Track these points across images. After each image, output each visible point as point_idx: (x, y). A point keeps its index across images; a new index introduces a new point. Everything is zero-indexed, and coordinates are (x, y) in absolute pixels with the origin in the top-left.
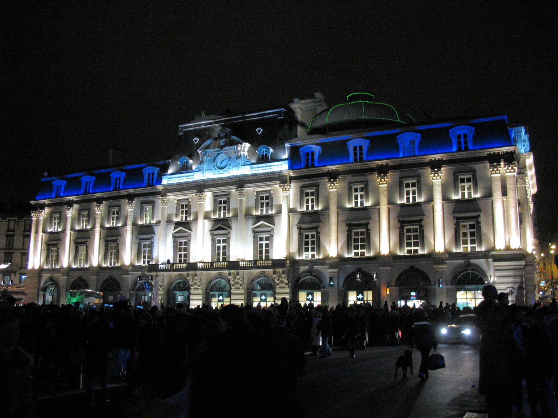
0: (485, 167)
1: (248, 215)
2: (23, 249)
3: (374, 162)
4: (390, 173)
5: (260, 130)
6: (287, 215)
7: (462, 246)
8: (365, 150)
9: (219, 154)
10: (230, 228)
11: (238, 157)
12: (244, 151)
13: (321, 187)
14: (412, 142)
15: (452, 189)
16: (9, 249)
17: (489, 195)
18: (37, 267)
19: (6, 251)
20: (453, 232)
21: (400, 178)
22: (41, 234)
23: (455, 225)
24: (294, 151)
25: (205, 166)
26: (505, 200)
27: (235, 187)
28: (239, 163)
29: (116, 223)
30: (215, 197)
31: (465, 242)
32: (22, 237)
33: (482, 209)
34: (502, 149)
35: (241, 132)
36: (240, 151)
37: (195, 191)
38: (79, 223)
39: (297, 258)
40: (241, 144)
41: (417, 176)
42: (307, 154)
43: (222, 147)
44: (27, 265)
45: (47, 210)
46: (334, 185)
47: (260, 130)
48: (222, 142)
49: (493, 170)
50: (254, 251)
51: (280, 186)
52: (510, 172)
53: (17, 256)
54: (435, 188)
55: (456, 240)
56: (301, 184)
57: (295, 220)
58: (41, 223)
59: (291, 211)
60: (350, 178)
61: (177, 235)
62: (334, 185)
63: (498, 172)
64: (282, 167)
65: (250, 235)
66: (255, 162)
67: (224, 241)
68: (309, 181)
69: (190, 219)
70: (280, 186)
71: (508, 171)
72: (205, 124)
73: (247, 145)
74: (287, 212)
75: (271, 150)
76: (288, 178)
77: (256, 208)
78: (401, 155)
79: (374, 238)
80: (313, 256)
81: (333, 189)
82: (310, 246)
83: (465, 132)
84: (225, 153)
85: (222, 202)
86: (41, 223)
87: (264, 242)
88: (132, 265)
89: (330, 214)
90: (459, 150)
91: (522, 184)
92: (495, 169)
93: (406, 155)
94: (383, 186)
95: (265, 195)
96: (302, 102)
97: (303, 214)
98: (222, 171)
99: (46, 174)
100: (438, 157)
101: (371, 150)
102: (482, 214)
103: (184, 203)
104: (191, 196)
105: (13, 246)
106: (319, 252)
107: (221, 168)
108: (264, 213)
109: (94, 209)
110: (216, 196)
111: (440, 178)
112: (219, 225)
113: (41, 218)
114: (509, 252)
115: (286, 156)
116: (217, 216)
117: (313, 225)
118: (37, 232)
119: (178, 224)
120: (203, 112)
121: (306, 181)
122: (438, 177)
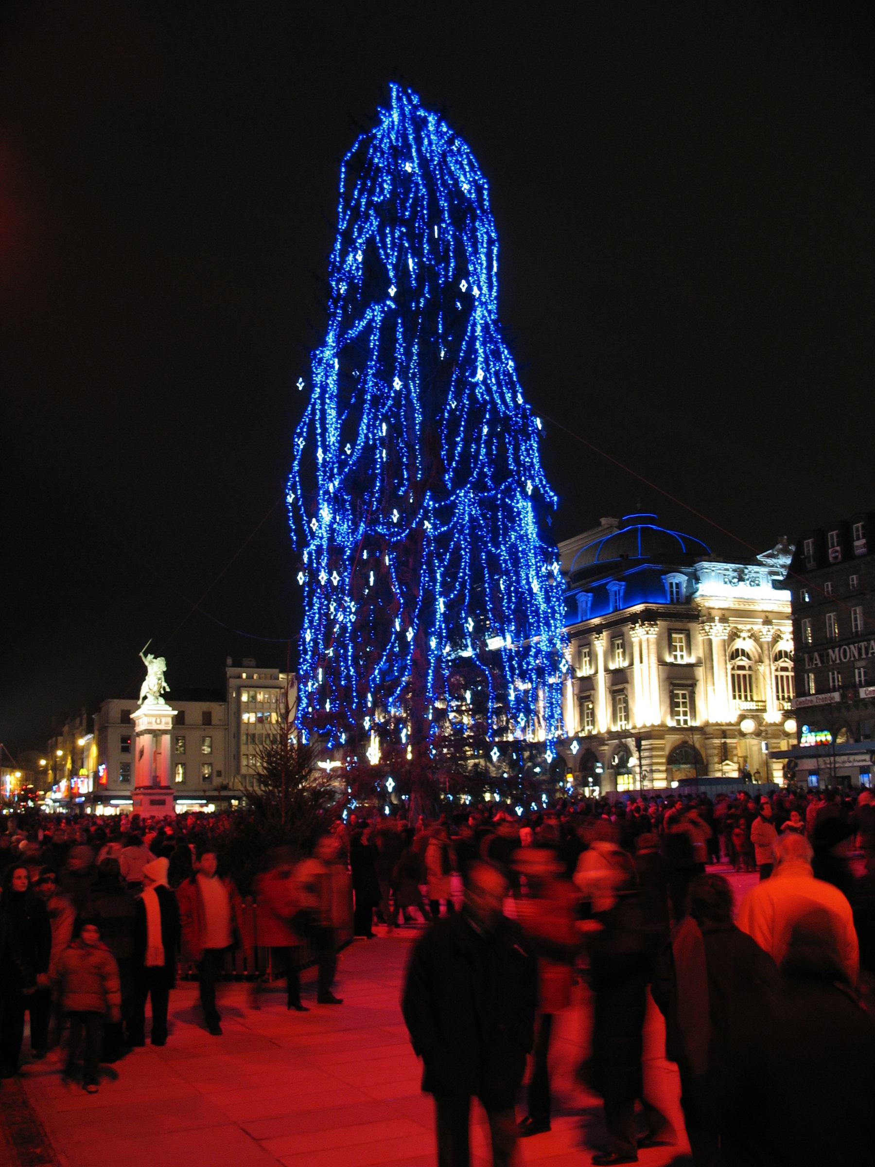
78: (580, 620)
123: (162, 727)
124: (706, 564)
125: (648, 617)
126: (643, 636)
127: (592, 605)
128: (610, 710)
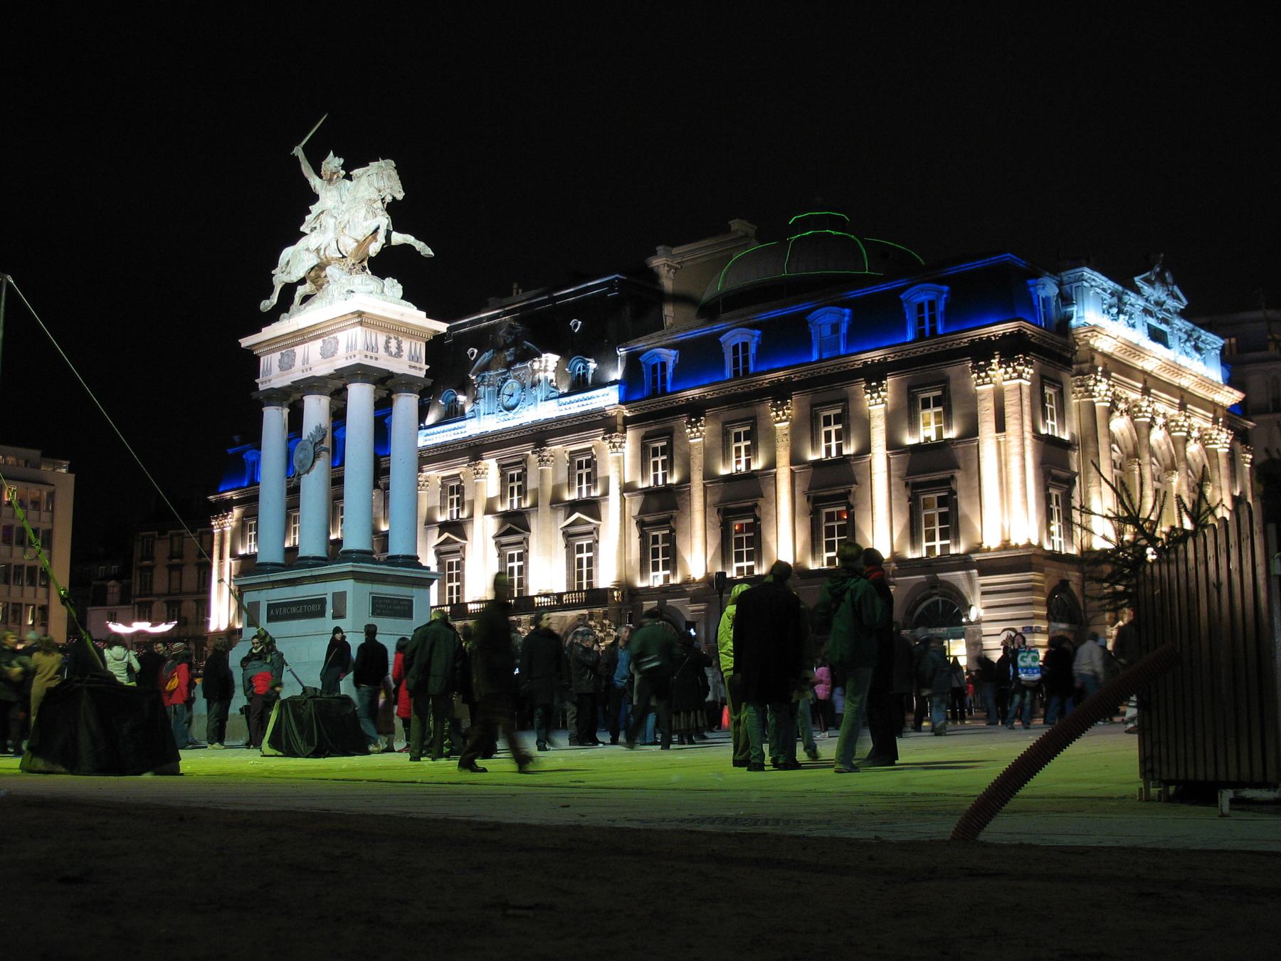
0: (964, 371)
1: (556, 501)
2: (198, 593)
3: (856, 357)
4: (889, 380)
5: (577, 325)
6: (618, 497)
7: (925, 544)
8: (752, 350)
9: (505, 380)
10: (529, 530)
11: (534, 385)
12: (545, 371)
13: (676, 434)
14: (835, 328)
15: (906, 424)
16: (146, 596)
17: (971, 432)
18: (224, 627)
19: (168, 598)
20: (907, 515)
21: (813, 406)
22: (227, 559)
23: (910, 500)
24: (633, 362)
25: (482, 406)
26: (1002, 439)
27: (531, 445)
28: (536, 398)
29: (589, 489)
30: (503, 468)
31: (931, 537)
32: (166, 572)
33: (962, 465)
34: (994, 328)
35: (542, 333)
36: (539, 370)
37: (466, 459)
38: (726, 458)
39: (640, 584)
40: (540, 356)
41: (841, 401)
42: (655, 366)
43: (509, 366)
44: (208, 622)
45: (237, 512)
46: (879, 396)
47: (577, 325)
48: (508, 355)
49: (979, 377)
50: (568, 575)
51: (604, 439)
52: (1011, 378)
53: (189, 606)
54: (873, 424)
55: (913, 534)
56: (642, 431)
57: (634, 506)
58: (228, 537)
59: (627, 488)
60: (727, 414)
61: (443, 548)
62: (879, 396)
63: (987, 380)
64: (607, 399)
65: (561, 542)
66: (566, 391)
67: (521, 557)
68: (656, 423)
69: (464, 515)
70: (604, 439)
71: (1007, 376)
72: (490, 318)
73: (551, 360)
74: (618, 492)
75: (592, 365)
76: (620, 421)
77: (570, 486)
78: (815, 357)
79: (769, 537)
80: (666, 578)
81: (697, 437)
82: (937, 528)
83: (931, 297)
84: (515, 377)
85: (513, 478)
86: (228, 537)
87: (585, 555)
88: (626, 588)
89: (778, 477)
90: (920, 336)
91: (1083, 397)
92: (983, 375)
93: (825, 356)
94: (782, 427)
95: (584, 459)
96: (676, 251)
97: (647, 492)
98: (511, 415)
99: (237, 438)
100: (876, 356)
101: (765, 352)
102: (958, 474)
103: (455, 484)
104: (461, 468)
105: (151, 589)
106: (674, 572)
107: (509, 409)
108: (584, 495)
109: (862, 400)
110: (504, 466)
111: (883, 402)
112: (508, 526)
113: (228, 529)
114: (1005, 554)
115: (617, 374)
116: (507, 507)
117: (662, 516)
118: (221, 557)
119: (444, 527)
120: (515, 286)
121: (650, 425)
122: (879, 400)
123: (400, 366)
124: (1087, 272)
125: (1010, 349)
126: (1006, 381)
127: (849, 329)
128: (714, 542)
